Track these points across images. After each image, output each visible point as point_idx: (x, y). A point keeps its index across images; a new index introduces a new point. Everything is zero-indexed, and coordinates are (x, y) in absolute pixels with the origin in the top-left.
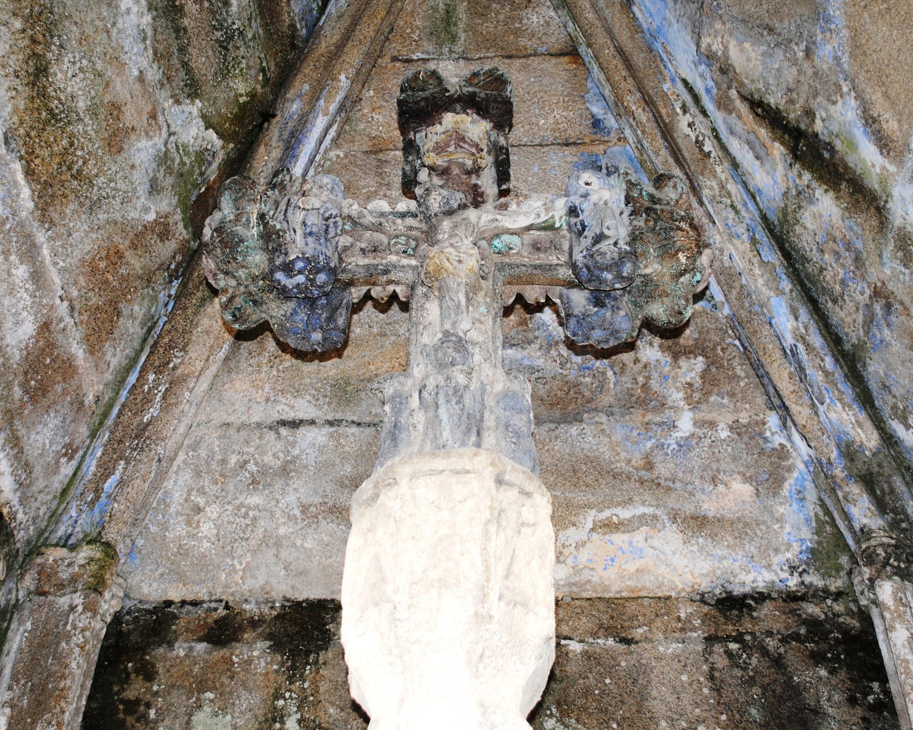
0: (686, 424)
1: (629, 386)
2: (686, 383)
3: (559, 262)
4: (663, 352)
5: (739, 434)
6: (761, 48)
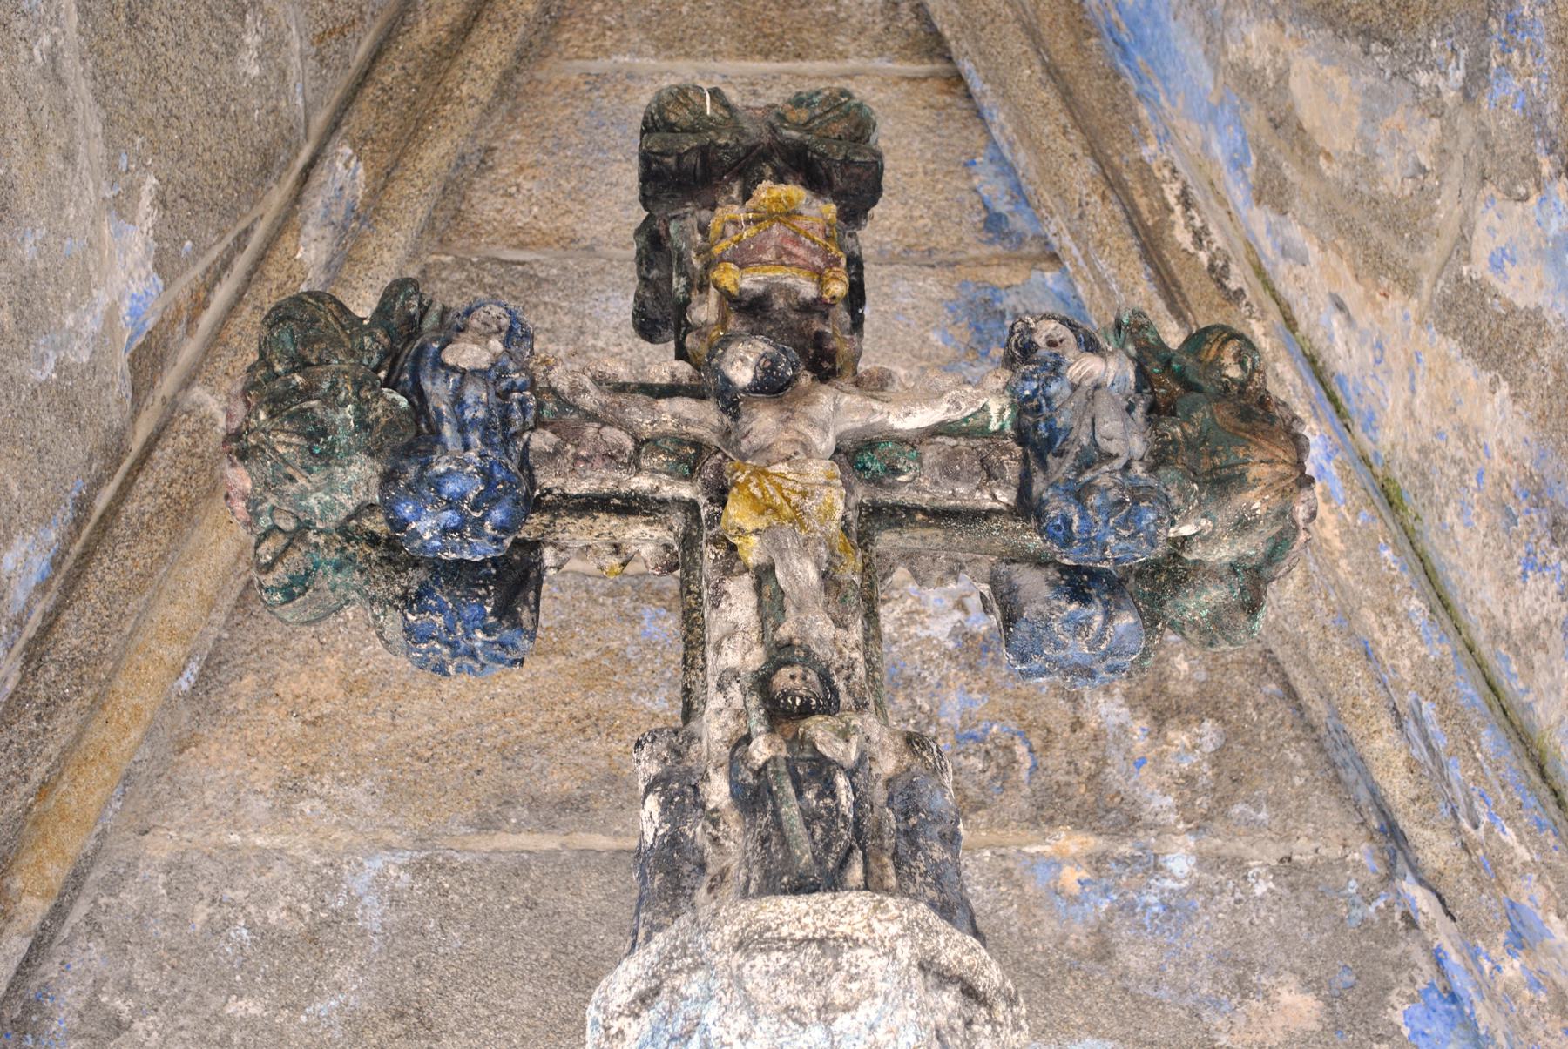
0: (1180, 862)
1: (1062, 778)
2: (1181, 776)
3: (997, 506)
4: (1133, 708)
5: (1293, 887)
6: (1363, 79)
